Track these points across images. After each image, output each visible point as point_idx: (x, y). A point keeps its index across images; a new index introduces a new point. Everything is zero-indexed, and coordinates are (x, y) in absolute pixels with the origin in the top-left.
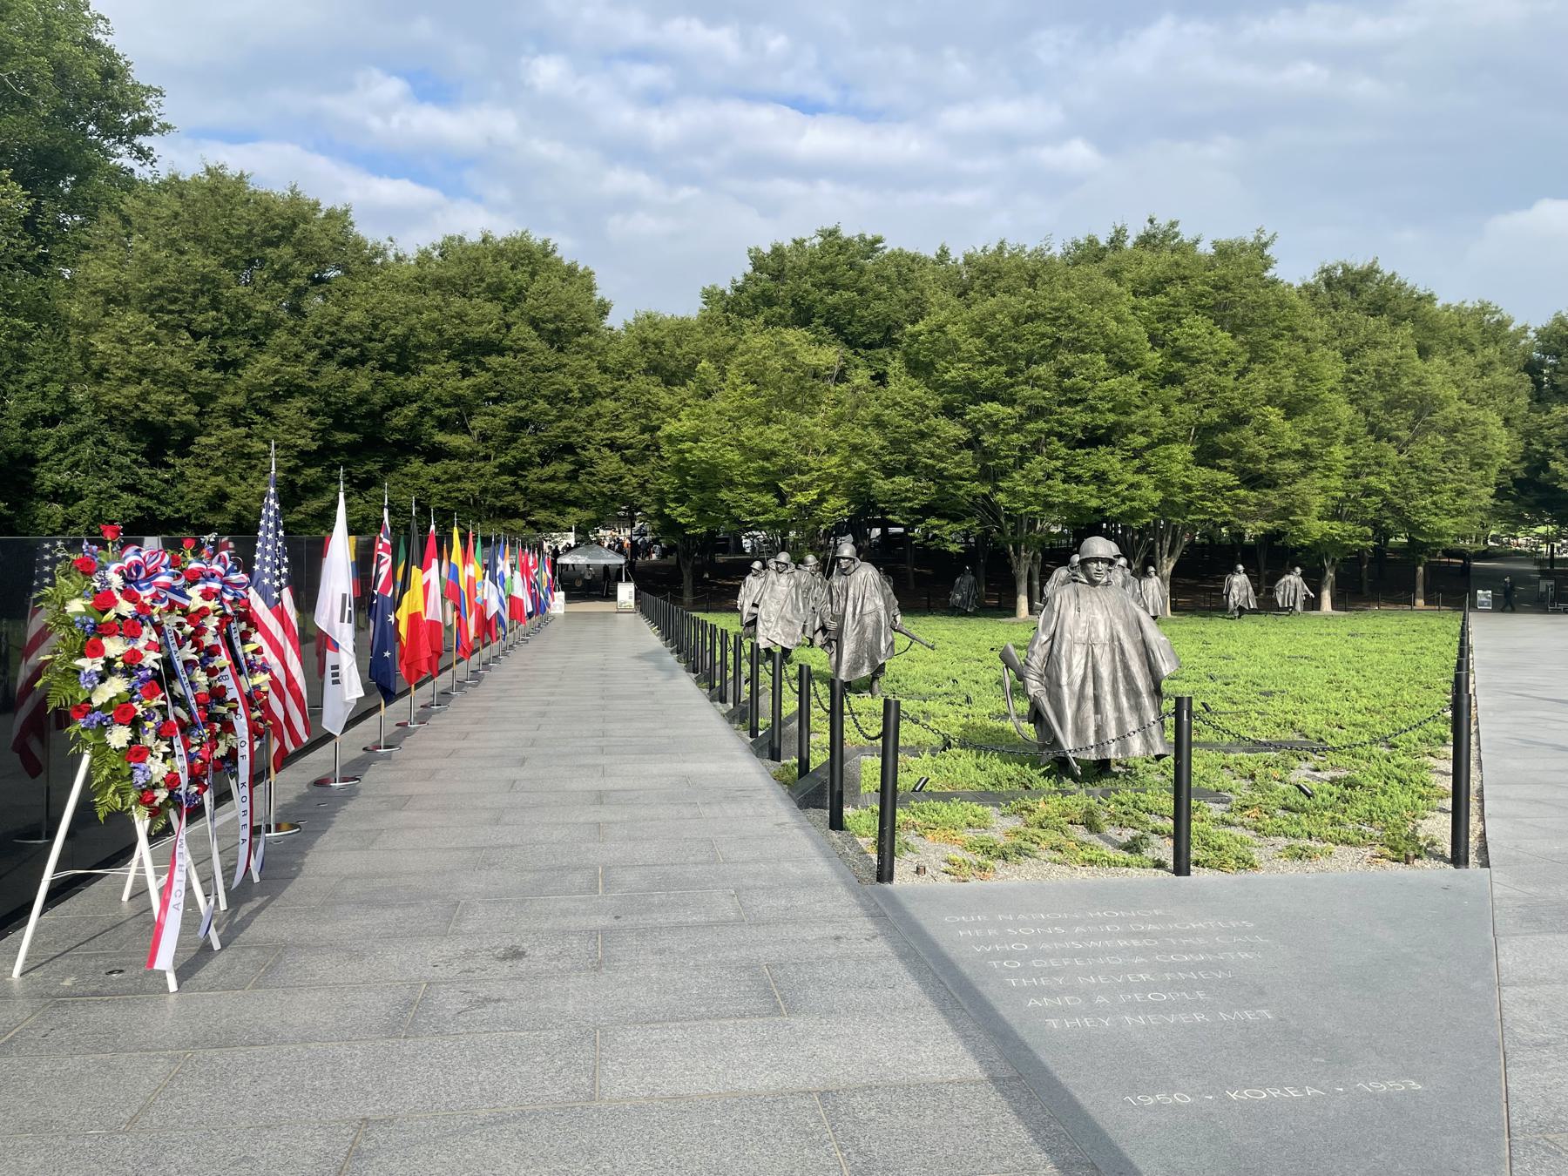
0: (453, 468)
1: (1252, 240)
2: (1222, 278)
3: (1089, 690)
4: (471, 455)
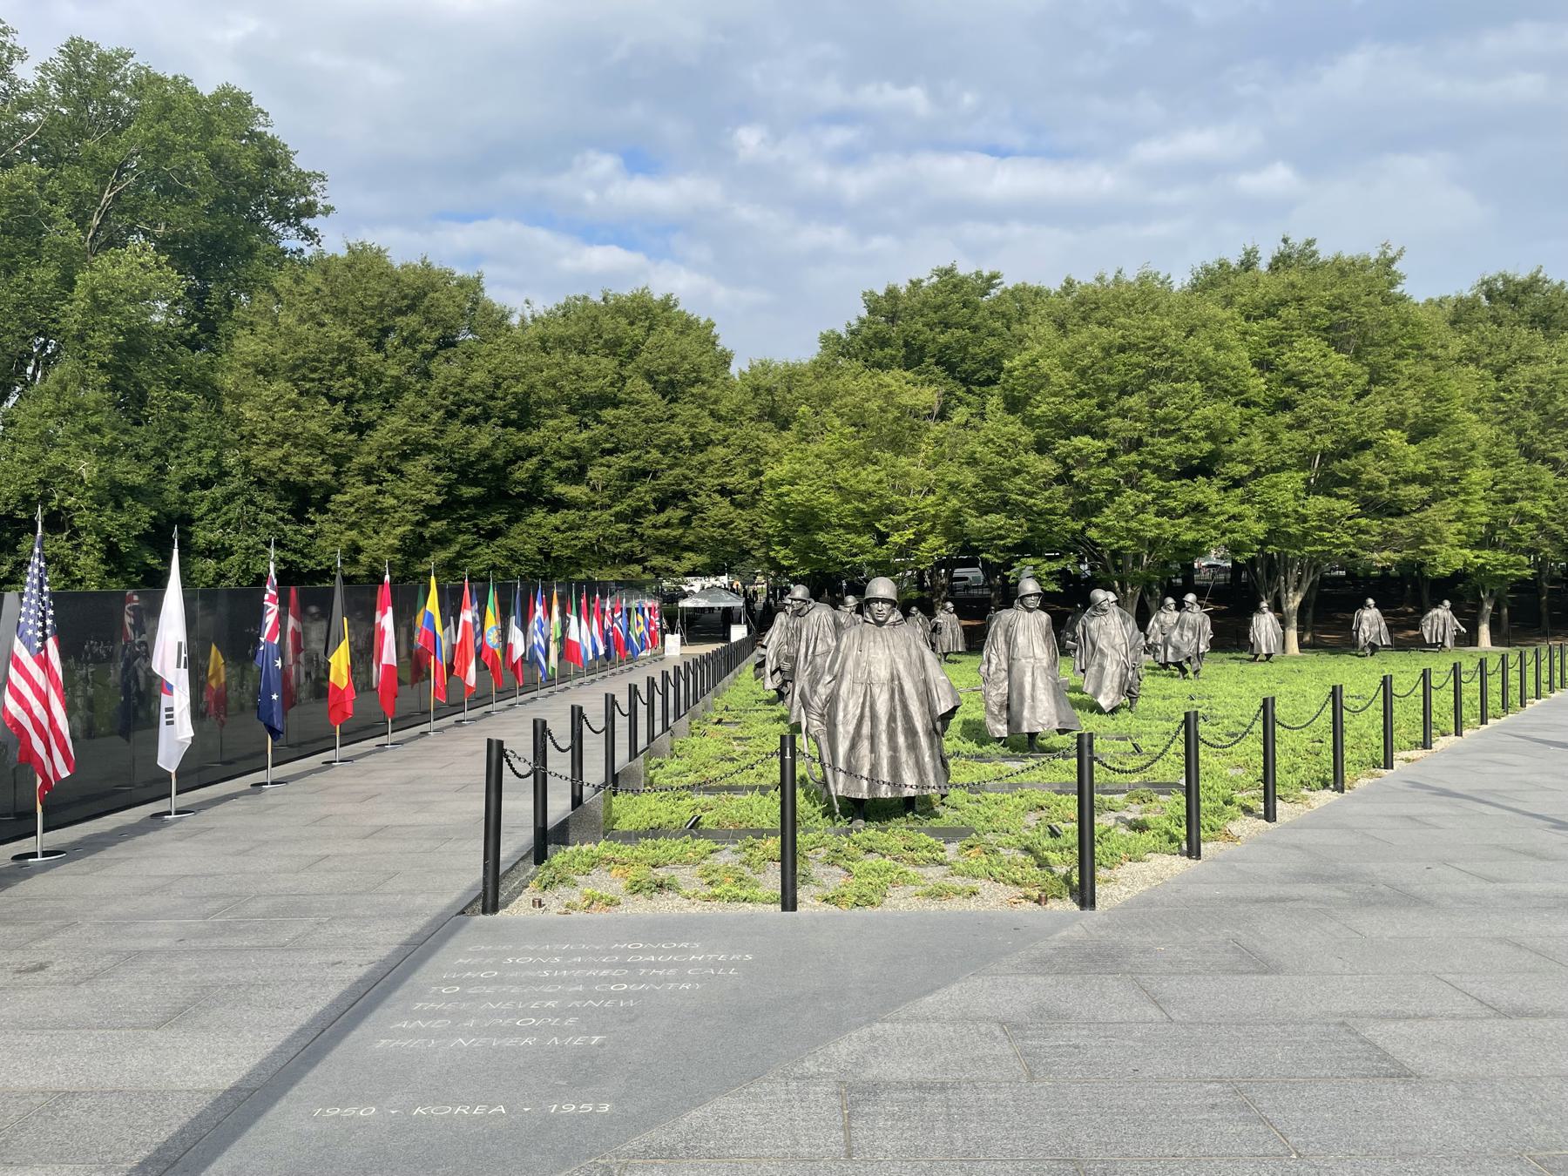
0: (571, 518)
1: (1377, 256)
2: (1339, 297)
3: (866, 729)
4: (591, 504)
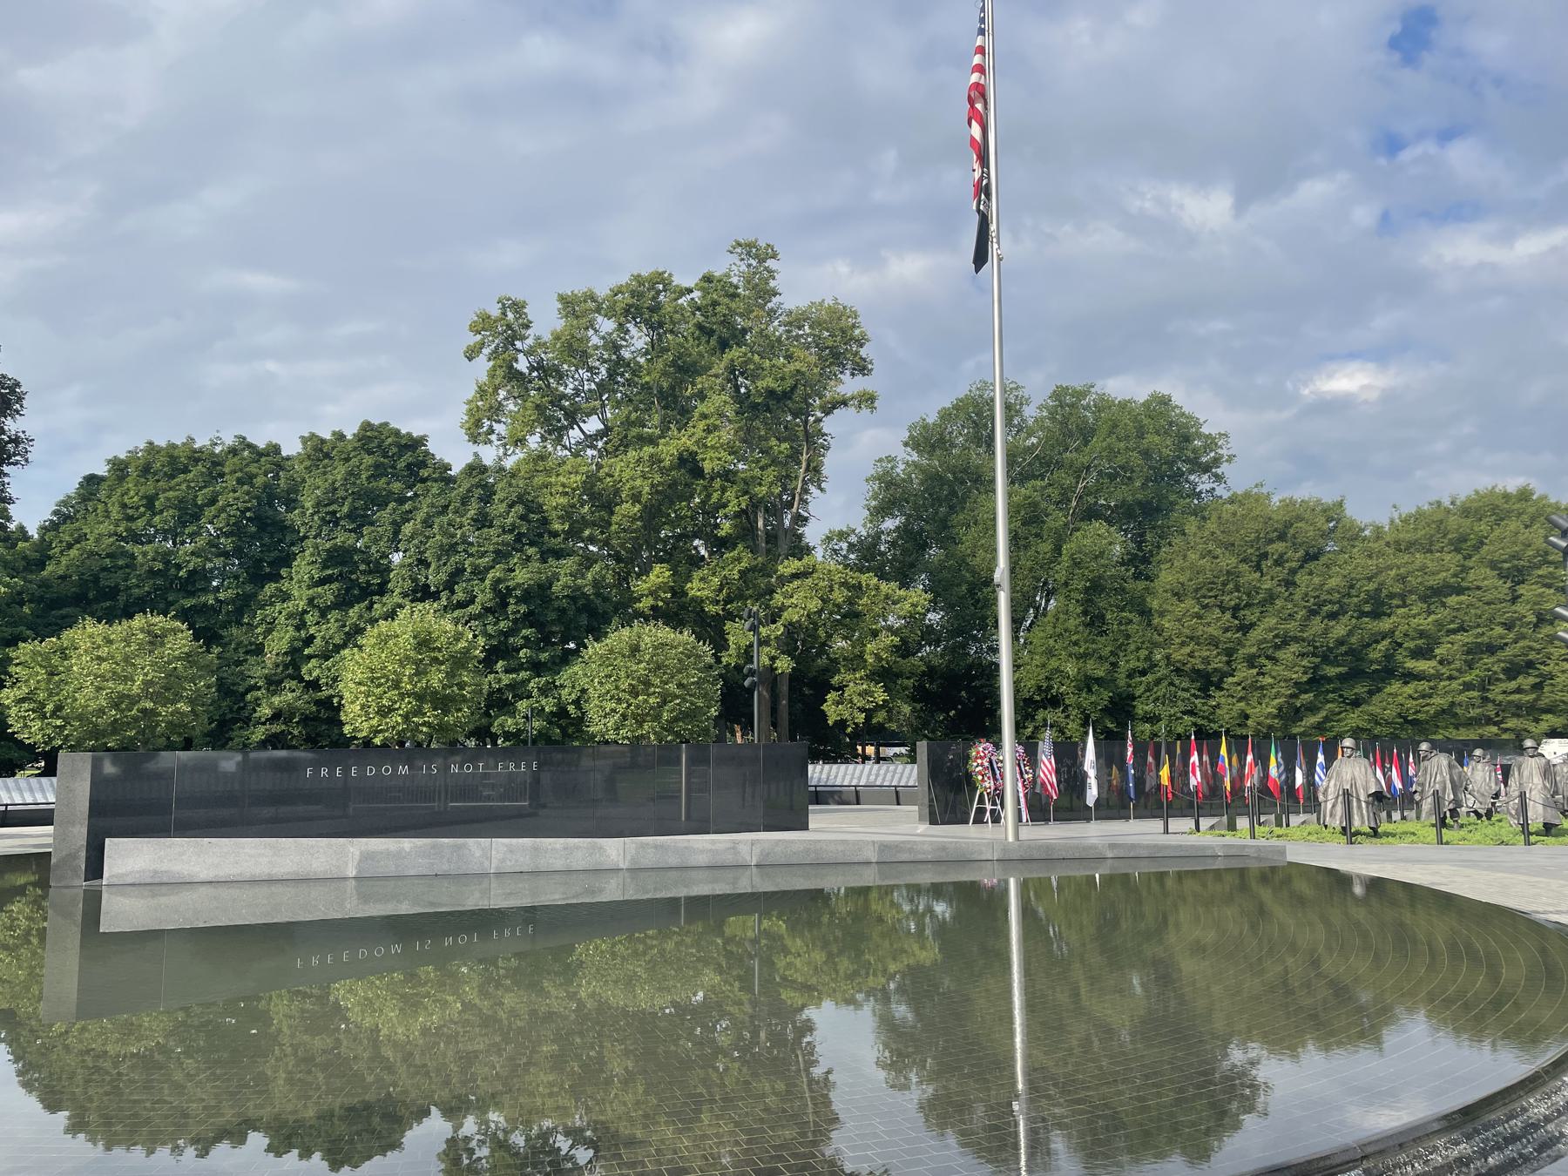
0: (1421, 688)
4: (1438, 676)
